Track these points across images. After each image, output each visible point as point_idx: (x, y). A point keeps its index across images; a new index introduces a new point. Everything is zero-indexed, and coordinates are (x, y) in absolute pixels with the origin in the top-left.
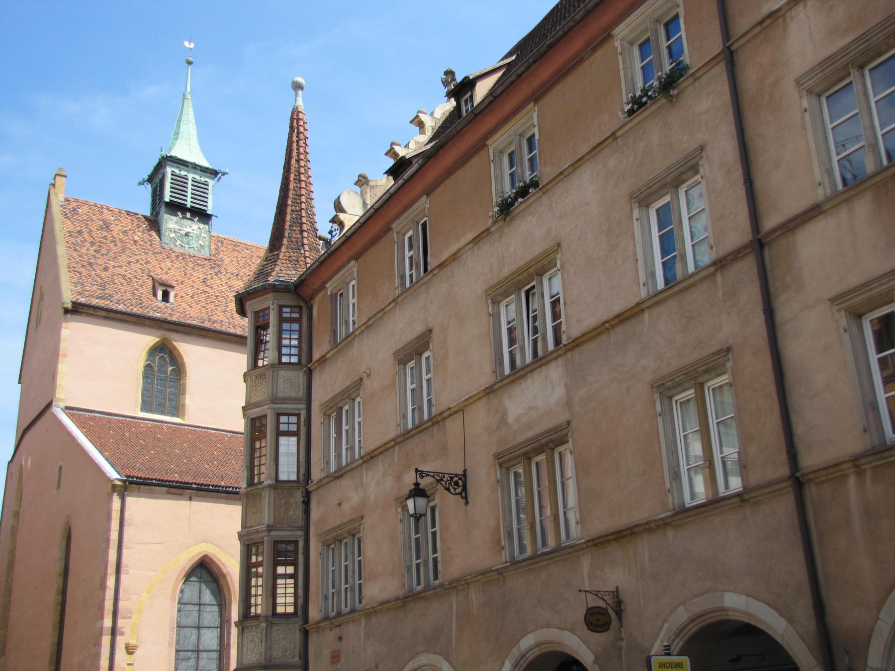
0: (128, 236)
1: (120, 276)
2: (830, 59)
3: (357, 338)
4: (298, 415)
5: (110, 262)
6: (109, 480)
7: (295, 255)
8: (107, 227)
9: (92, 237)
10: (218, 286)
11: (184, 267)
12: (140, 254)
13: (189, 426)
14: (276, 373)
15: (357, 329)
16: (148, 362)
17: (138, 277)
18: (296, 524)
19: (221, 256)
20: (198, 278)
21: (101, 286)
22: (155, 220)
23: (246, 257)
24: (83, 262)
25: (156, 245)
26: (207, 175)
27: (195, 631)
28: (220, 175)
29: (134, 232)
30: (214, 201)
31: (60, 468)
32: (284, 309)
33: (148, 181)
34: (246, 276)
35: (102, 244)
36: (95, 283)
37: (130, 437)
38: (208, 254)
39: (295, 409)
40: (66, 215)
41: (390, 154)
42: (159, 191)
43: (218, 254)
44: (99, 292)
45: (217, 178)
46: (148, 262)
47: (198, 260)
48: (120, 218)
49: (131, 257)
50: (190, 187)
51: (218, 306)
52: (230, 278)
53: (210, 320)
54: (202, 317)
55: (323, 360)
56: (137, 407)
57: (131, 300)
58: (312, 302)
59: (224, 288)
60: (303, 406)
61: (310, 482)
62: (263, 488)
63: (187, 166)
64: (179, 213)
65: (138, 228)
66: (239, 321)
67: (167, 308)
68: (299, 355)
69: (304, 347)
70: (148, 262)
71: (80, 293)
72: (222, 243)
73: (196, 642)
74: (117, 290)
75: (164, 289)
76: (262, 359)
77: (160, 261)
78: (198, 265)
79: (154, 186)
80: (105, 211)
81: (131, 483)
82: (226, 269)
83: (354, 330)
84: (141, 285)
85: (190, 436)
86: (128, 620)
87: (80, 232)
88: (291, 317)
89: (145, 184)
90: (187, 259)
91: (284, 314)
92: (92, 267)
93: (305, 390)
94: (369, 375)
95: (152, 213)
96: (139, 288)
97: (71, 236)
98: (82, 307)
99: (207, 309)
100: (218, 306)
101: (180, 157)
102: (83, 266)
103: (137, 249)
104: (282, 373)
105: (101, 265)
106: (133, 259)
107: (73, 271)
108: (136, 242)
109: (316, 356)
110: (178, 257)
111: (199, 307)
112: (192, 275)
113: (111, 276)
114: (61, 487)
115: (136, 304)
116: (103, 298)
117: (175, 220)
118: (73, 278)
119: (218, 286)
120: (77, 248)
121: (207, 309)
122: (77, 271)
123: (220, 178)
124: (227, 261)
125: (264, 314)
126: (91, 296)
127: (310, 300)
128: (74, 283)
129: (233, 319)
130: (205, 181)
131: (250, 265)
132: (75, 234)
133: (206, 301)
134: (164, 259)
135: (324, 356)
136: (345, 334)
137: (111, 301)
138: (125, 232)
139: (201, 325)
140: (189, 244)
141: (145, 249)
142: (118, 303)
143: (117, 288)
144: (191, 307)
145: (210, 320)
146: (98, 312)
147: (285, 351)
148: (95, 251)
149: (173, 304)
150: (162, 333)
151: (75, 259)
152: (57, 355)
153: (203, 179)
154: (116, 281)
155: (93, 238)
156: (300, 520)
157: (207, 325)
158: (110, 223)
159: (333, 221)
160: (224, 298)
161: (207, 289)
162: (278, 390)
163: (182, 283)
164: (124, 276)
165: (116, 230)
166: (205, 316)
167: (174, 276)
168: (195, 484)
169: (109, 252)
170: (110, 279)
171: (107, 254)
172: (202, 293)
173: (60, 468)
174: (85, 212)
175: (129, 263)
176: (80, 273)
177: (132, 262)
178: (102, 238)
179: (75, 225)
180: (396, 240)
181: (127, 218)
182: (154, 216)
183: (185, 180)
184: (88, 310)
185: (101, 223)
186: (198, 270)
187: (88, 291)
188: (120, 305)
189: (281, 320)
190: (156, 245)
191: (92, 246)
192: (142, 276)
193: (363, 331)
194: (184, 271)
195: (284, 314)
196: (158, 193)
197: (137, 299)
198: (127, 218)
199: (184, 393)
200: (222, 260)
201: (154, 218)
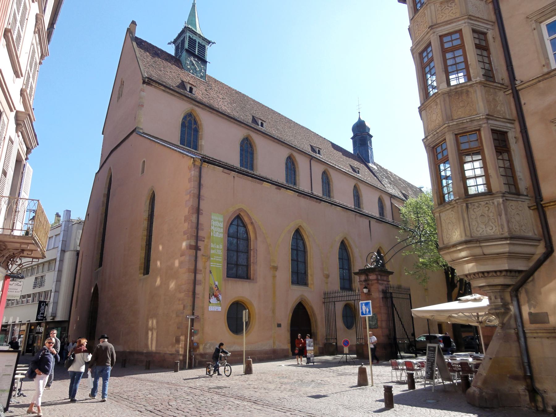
2: (457, 49)
27: (235, 241)
28: (211, 43)
33: (173, 43)
73: (236, 260)
150: (191, 106)
173: (144, 161)
184: (156, 84)
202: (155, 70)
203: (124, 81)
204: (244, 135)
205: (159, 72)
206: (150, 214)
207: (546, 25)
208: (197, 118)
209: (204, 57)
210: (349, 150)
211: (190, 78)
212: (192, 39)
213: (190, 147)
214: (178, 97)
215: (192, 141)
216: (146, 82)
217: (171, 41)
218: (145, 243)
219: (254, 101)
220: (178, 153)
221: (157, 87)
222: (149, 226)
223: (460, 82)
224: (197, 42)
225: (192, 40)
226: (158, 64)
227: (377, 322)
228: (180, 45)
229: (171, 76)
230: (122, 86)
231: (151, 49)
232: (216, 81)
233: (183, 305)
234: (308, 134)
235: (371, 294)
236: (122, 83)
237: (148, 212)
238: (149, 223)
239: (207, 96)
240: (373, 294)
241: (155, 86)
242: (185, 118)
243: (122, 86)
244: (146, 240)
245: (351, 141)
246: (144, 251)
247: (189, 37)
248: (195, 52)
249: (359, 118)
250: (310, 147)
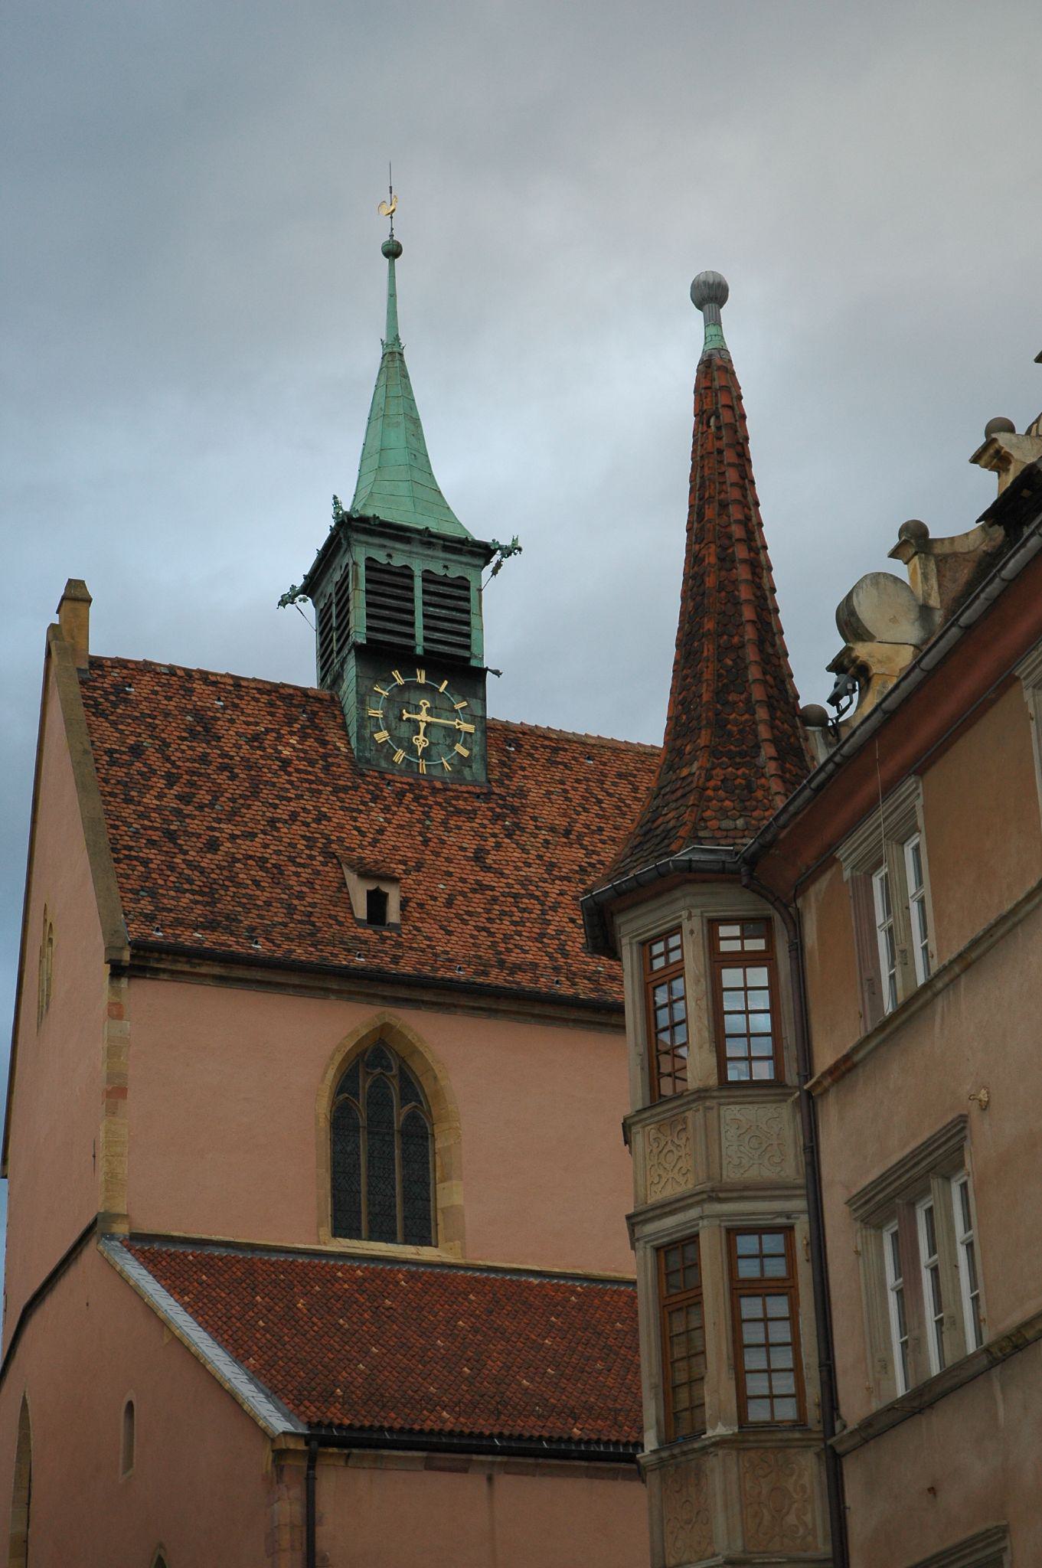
0: (264, 750)
1: (250, 862)
3: (940, 998)
4: (788, 1230)
5: (222, 826)
6: (264, 1433)
7: (740, 772)
8: (207, 730)
9: (168, 760)
10: (517, 868)
11: (419, 821)
12: (299, 797)
13: (467, 1268)
14: (714, 1113)
15: (939, 975)
16: (341, 1097)
17: (298, 860)
18: (809, 1554)
19: (517, 782)
20: (464, 849)
21: (201, 893)
22: (332, 698)
23: (588, 780)
24: (150, 832)
25: (339, 766)
26: (463, 559)
29: (279, 738)
31: (130, 1405)
32: (721, 929)
34: (593, 832)
35: (195, 778)
36: (186, 886)
37: (308, 1310)
38: (482, 778)
39: (779, 1214)
40: (97, 705)
41: (985, 458)
42: (337, 617)
43: (510, 778)
44: (199, 910)
45: (492, 566)
46: (321, 817)
47: (457, 798)
48: (236, 701)
49: (275, 806)
51: (521, 923)
52: (547, 841)
53: (502, 964)
54: (480, 957)
55: (844, 1069)
56: (320, 1225)
57: (285, 925)
58: (799, 902)
59: (535, 871)
60: (800, 1204)
61: (838, 1426)
62: (704, 1448)
63: (408, 541)
64: (396, 674)
65: (290, 724)
66: (584, 962)
67: (383, 939)
68: (776, 1058)
69: (789, 1034)
70: (321, 817)
71: (150, 918)
72: (519, 747)
74: (244, 901)
76: (669, 1075)
77: (355, 810)
78: (459, 812)
79: (322, 606)
80: (198, 686)
81: (326, 1442)
82: (534, 819)
83: (929, 978)
84: (310, 883)
85: (471, 1297)
87: (137, 751)
88: (743, 952)
89: (297, 599)
90: (426, 798)
91: (722, 943)
92: (175, 844)
93: (802, 1158)
94: (985, 1107)
95: (322, 680)
96: (305, 889)
97: (113, 763)
98: (156, 955)
99: (491, 934)
100: (521, 923)
101: (386, 516)
102: (151, 843)
103: (291, 782)
104: (732, 1113)
105: (199, 836)
106: (282, 813)
107: (127, 857)
108: (286, 763)
109: (825, 1058)
110: (400, 795)
111: (469, 929)
112: (443, 842)
113: (226, 864)
115: (300, 936)
116: (211, 926)
117: (385, 693)
118: (128, 877)
119: (517, 868)
120: (133, 793)
121: (491, 934)
122: (136, 858)
123: (499, 565)
124: (535, 794)
125: (666, 945)
126: (178, 922)
127: (795, 899)
128: (131, 891)
129: (565, 955)
130: (459, 578)
131: (600, 801)
132: (124, 757)
133: (488, 911)
134: (364, 803)
135: (847, 1057)
136: (905, 989)
137: (232, 934)
138: (256, 737)
139: (480, 980)
140: (430, 756)
141: (311, 782)
142: (251, 938)
143: (245, 896)
144: (450, 933)
145: (502, 964)
146: (199, 965)
147: (734, 1049)
148: (180, 798)
149: (395, 927)
151: (130, 825)
153: (454, 572)
154: (241, 876)
155: (173, 763)
156: (820, 1539)
157: (496, 978)
158: (213, 718)
159: (836, 666)
160: (537, 898)
161: (488, 879)
162: (725, 1163)
163: (419, 867)
164: (262, 861)
165: (230, 735)
166: (486, 954)
167: (395, 848)
168: (500, 1436)
169: (216, 798)
170: (226, 873)
171: (211, 805)
172: (474, 891)
173: (130, 1405)
174: (145, 692)
175: (272, 822)
176: (145, 863)
177: (279, 820)
178: (195, 761)
179: (121, 732)
180: (1031, 710)
181: (257, 700)
182: (330, 688)
183: (464, 616)
184: (175, 961)
185: (189, 718)
186: (459, 828)
187: (171, 910)
188: (256, 943)
189: (718, 960)
190: (339, 766)
191: (170, 786)
192: (311, 857)
193: (958, 976)
194: (421, 834)
195: (722, 943)
196: (334, 622)
197: (300, 922)
198: (257, 700)
200: (522, 793)
201: (328, 692)
208: (415, 1065)
212: (388, 570)
213: (390, 1238)
214: (295, 986)
215: (398, 1200)
216: (124, 968)
221: (182, 972)
223: (758, 1301)
224: (418, 573)
225: (386, 578)
241: (172, 972)
242: (347, 1083)
248: (412, 636)
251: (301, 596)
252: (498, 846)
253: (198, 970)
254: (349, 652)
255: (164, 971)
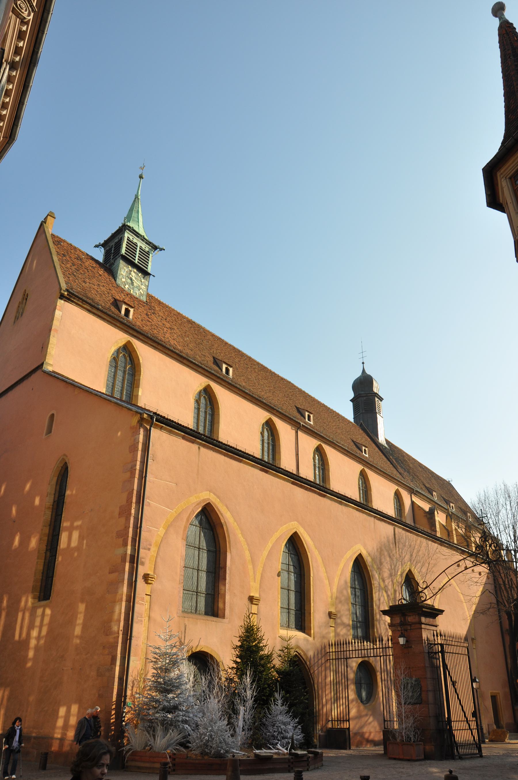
30: (152, 266)
31: (52, 416)
42: (114, 250)
50: (138, 252)
75: (127, 307)
86: (147, 551)
98: (74, 297)
114: (53, 431)
146: (85, 304)
152: (50, 330)
173: (52, 416)
184: (78, 300)
199: (138, 387)
202: (77, 281)
203: (27, 294)
204: (201, 384)
205: (84, 284)
206: (56, 499)
207: (129, 341)
209: (147, 268)
210: (349, 419)
211: (124, 295)
217: (100, 243)
218: (45, 547)
219: (213, 335)
220: (113, 404)
222: (53, 520)
224: (139, 246)
226: (81, 273)
227: (420, 694)
228: (113, 249)
229: (98, 290)
230: (25, 301)
231: (72, 251)
232: (160, 303)
233: (111, 657)
234: (291, 390)
235: (411, 647)
236: (25, 297)
237: (53, 496)
238: (54, 514)
239: (148, 323)
240: (413, 646)
243: (25, 301)
244: (46, 542)
245: (351, 404)
246: (43, 561)
247: (128, 239)
248: (135, 260)
249: (364, 370)
250: (295, 409)
251: (101, 247)
252: (151, 315)
253: (84, 305)
254: (119, 257)
255: (74, 302)
